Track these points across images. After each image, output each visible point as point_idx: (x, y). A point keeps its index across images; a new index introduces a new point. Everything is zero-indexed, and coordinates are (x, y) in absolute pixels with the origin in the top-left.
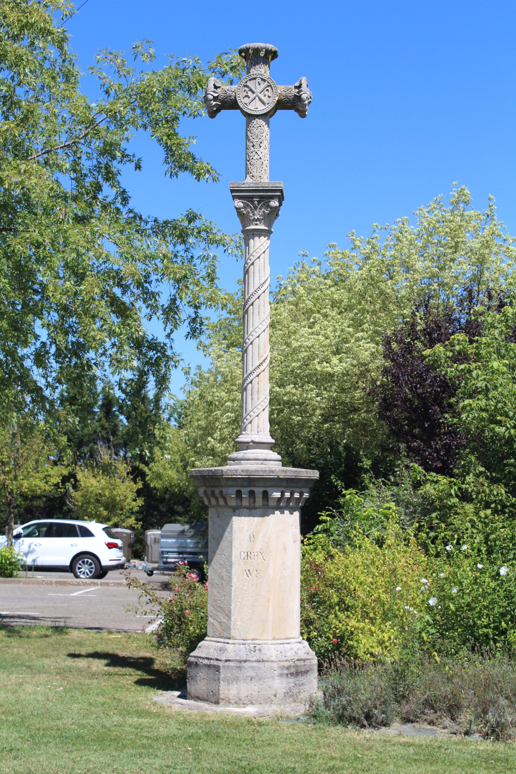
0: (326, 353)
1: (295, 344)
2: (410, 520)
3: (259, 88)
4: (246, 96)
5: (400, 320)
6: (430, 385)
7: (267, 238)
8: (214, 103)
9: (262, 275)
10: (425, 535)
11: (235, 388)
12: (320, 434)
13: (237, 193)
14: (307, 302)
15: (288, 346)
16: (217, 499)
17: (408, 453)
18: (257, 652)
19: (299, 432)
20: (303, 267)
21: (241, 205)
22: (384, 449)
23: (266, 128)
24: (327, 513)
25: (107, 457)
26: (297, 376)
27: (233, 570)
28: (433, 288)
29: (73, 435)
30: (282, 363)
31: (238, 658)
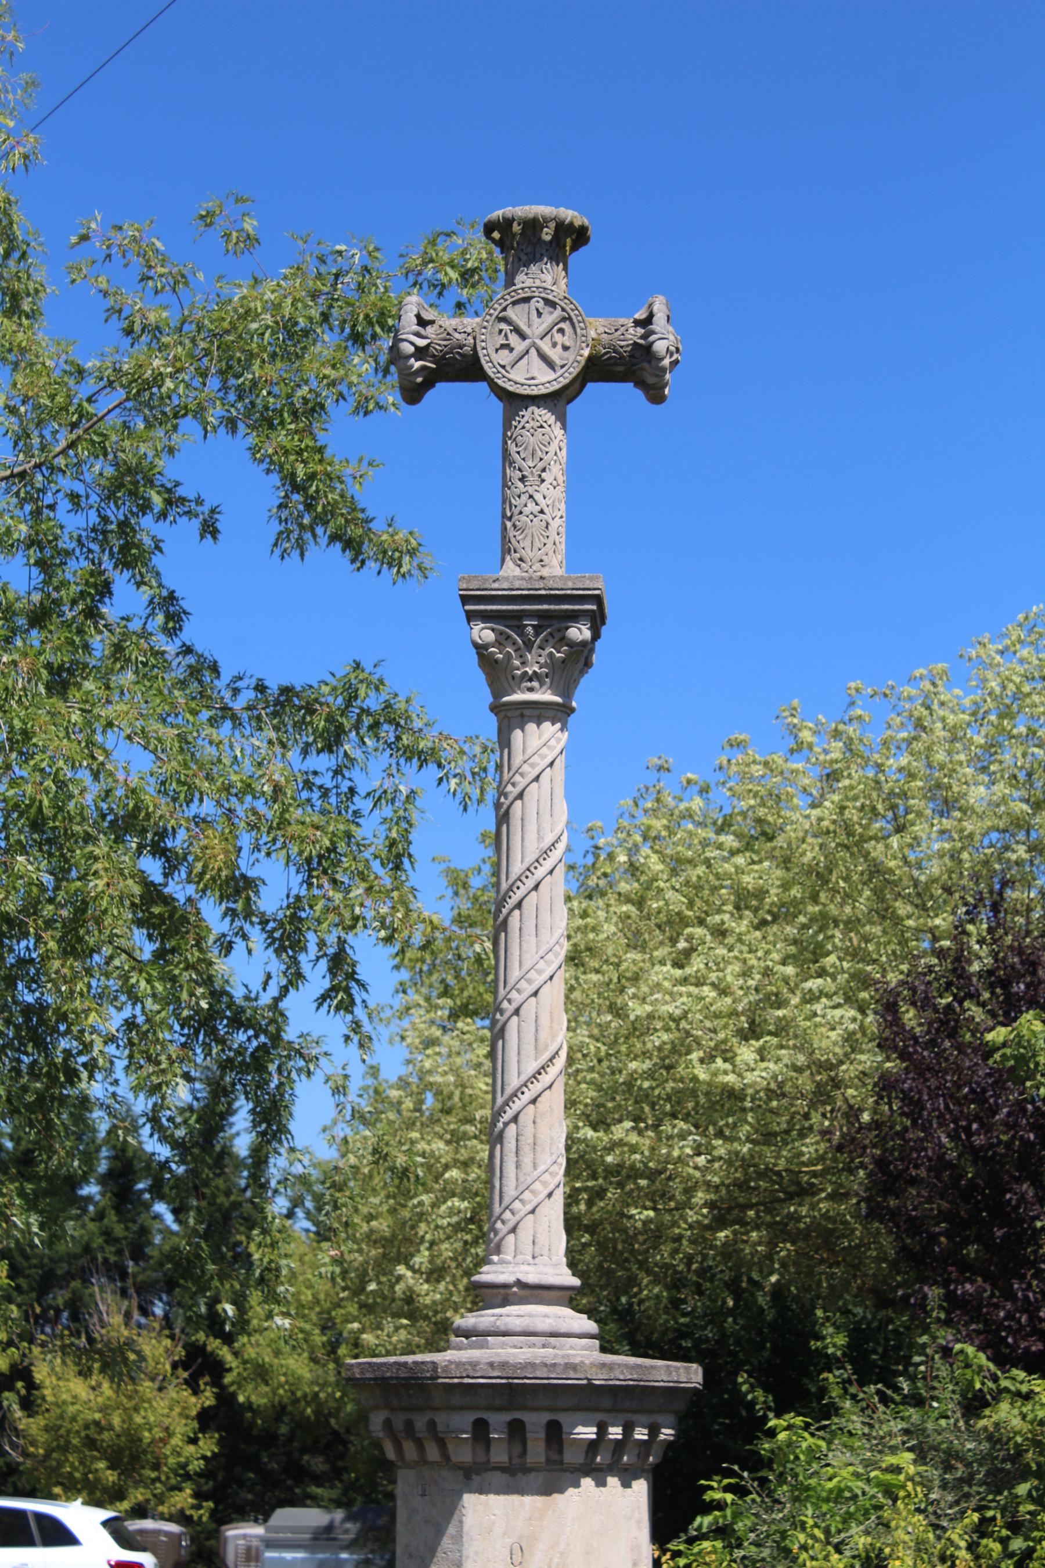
0: (721, 1036)
1: (637, 1010)
2: (957, 1503)
3: (540, 326)
4: (503, 346)
5: (926, 945)
6: (1005, 1123)
7: (558, 725)
8: (417, 365)
9: (546, 825)
10: (997, 1547)
11: (470, 1129)
12: (705, 1257)
13: (476, 605)
14: (670, 894)
15: (618, 1015)
16: (419, 1444)
17: (948, 1312)
19: (647, 1251)
20: (658, 800)
21: (489, 636)
22: (883, 1300)
23: (558, 431)
24: (726, 1481)
25: (117, 1320)
26: (644, 1097)
28: (1014, 857)
29: (27, 1258)
30: (600, 1061)
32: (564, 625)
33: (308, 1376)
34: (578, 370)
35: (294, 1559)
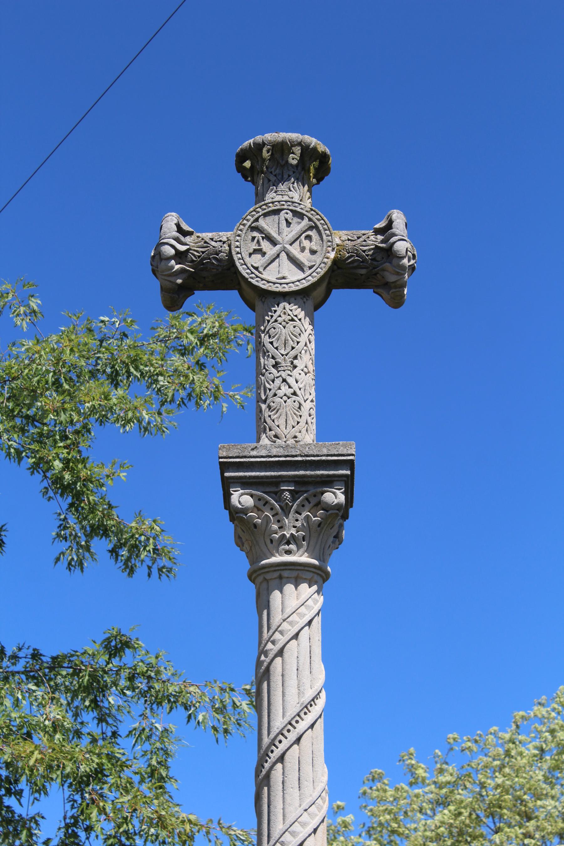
4: (256, 251)
7: (315, 588)
9: (306, 681)
32: (320, 490)
34: (325, 270)
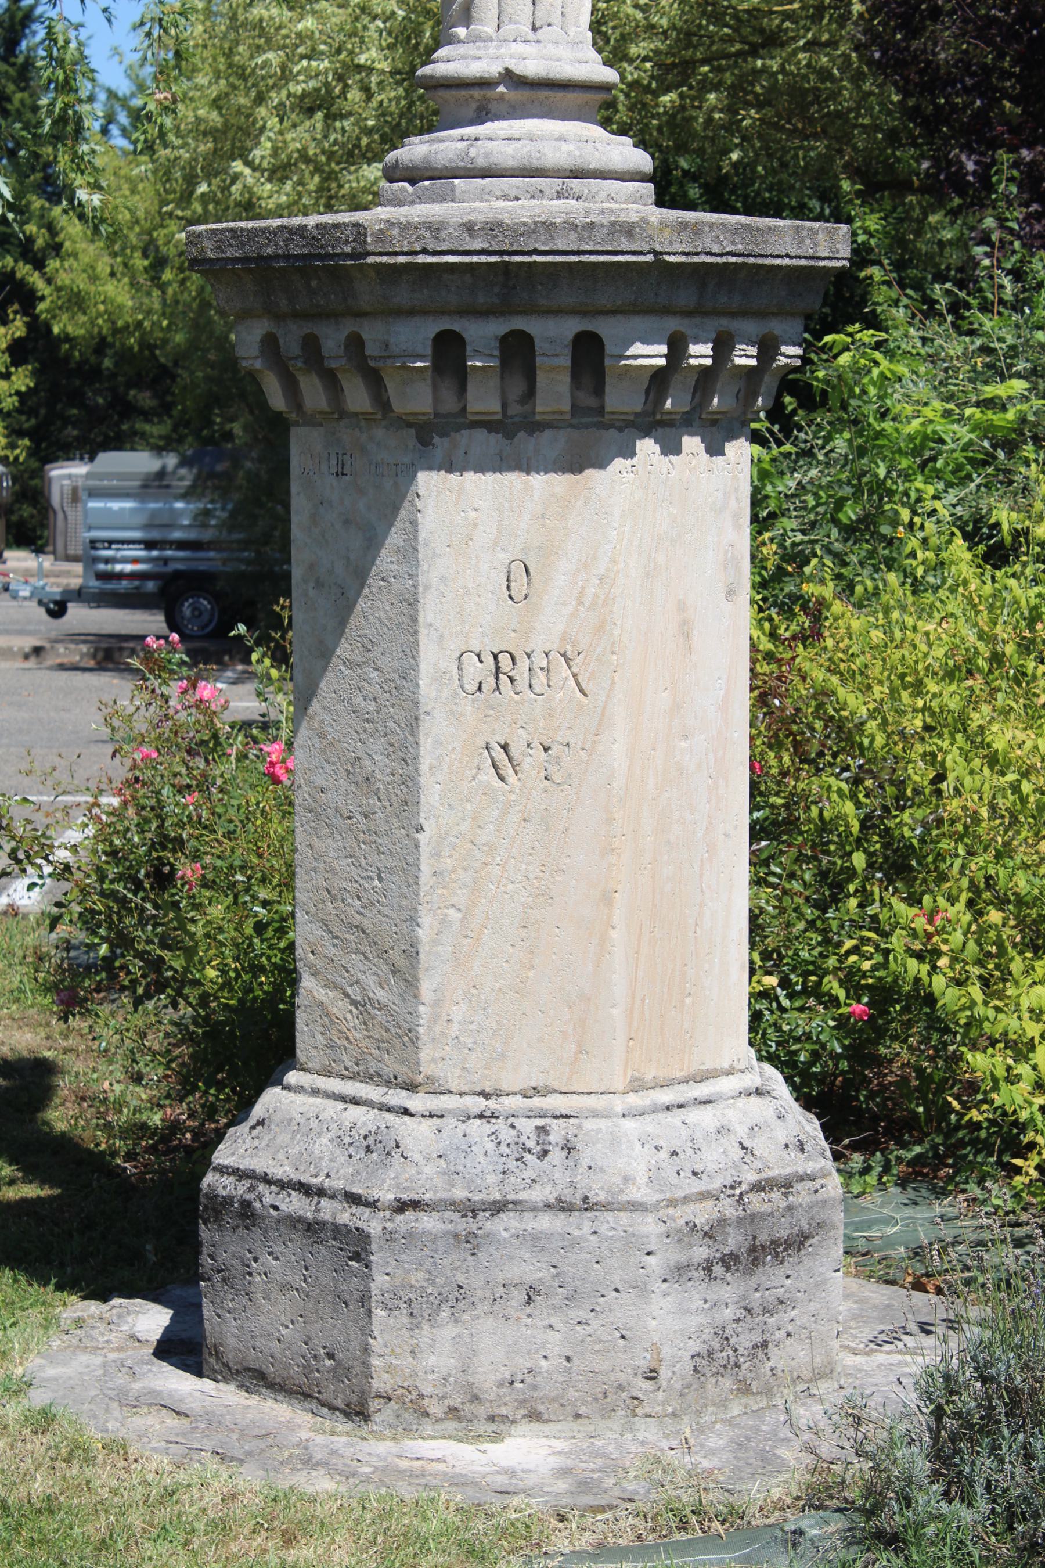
16: (331, 380)
18: (556, 1156)
27: (426, 745)
31: (459, 1193)
33: (130, 303)
35: (122, 509)
